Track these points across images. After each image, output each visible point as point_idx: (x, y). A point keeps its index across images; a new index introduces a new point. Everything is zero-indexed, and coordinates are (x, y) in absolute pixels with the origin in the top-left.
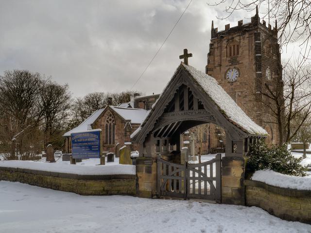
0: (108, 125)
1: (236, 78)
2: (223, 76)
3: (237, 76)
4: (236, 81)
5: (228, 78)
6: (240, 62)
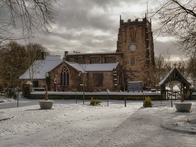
0: (63, 73)
1: (135, 50)
3: (136, 49)
4: (135, 51)
6: (137, 41)
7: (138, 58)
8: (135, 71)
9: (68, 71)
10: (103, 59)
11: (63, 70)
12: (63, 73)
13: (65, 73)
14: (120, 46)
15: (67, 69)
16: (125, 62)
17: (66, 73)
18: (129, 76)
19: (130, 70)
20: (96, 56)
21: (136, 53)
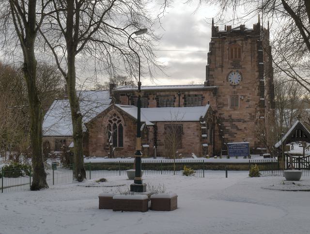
2: (226, 78)
3: (240, 80)
5: (230, 81)
6: (243, 66)
7: (244, 96)
8: (239, 121)
9: (120, 121)
10: (181, 98)
11: (112, 119)
12: (112, 125)
13: (115, 124)
14: (212, 75)
15: (118, 117)
16: (220, 104)
17: (118, 125)
18: (227, 128)
19: (228, 118)
20: (167, 93)
21: (241, 87)
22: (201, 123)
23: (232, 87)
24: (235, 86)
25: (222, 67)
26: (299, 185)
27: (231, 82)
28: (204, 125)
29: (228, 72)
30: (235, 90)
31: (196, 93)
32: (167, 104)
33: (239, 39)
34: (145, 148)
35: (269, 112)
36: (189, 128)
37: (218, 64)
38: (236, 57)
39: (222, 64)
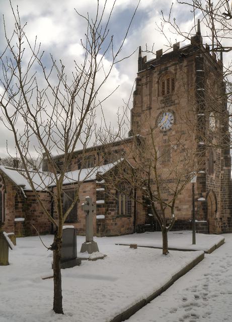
3: (172, 122)
6: (176, 102)
10: (101, 157)
21: (174, 133)
22: (97, 182)
23: (162, 135)
24: (165, 132)
25: (150, 108)
26: (195, 310)
27: (161, 128)
28: (101, 186)
29: (157, 115)
30: (166, 138)
31: (116, 148)
32: (89, 165)
33: (171, 63)
34: (19, 222)
35: (222, 172)
36: (84, 192)
37: (146, 106)
38: (168, 92)
39: (150, 104)
